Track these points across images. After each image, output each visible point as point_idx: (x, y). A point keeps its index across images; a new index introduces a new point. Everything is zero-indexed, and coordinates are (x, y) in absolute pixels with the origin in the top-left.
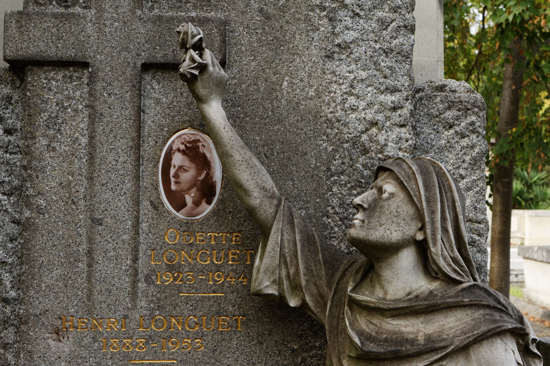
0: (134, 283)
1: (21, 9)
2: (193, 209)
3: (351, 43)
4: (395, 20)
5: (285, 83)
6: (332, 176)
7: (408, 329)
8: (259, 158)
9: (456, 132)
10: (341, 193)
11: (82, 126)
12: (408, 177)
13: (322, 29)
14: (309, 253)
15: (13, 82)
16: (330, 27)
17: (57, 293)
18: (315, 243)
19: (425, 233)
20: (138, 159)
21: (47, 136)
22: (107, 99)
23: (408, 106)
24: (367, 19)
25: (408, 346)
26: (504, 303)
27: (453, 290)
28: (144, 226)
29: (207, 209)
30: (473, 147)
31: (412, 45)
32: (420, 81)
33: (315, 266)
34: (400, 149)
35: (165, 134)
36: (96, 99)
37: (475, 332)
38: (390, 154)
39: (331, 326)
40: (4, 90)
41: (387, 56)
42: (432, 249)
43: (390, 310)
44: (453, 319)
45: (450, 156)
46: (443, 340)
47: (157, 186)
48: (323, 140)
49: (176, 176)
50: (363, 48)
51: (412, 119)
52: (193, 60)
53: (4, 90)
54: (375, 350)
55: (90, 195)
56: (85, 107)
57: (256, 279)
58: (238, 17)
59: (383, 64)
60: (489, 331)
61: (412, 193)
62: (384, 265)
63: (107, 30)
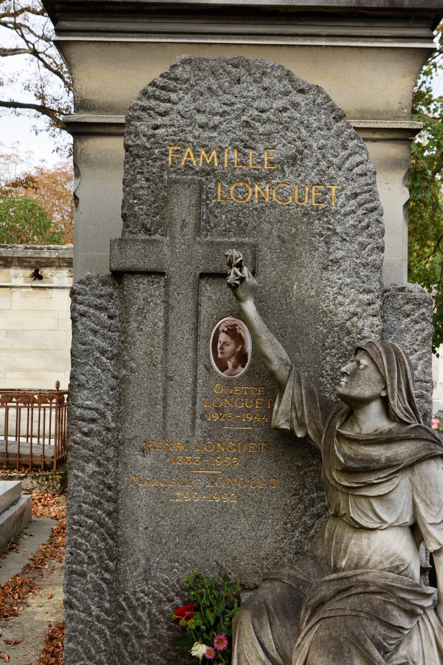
0: (193, 420)
1: (121, 237)
2: (233, 371)
3: (340, 259)
4: (370, 243)
5: (295, 286)
6: (326, 350)
7: (375, 453)
8: (277, 337)
9: (412, 320)
10: (332, 362)
11: (160, 314)
12: (377, 355)
13: (320, 249)
14: (311, 403)
15: (114, 284)
16: (326, 248)
17: (143, 425)
18: (315, 395)
19: (387, 392)
20: (197, 337)
21: (137, 321)
22: (177, 297)
23: (379, 302)
24: (351, 242)
25: (375, 464)
26: (439, 438)
27: (405, 429)
28: (200, 381)
29: (242, 371)
30: (423, 330)
31: (382, 261)
32: (387, 285)
33: (315, 411)
34: (373, 332)
35: (214, 320)
36: (169, 297)
37: (418, 456)
38: (366, 335)
39: (325, 450)
40: (108, 289)
41: (365, 268)
42: (391, 402)
43: (364, 440)
44: (404, 447)
45: (408, 336)
46: (397, 460)
47: (209, 355)
48: (320, 325)
49: (222, 348)
50: (349, 262)
51: (381, 311)
52: (236, 274)
53: (108, 289)
54: (354, 466)
55: (165, 361)
56: (162, 302)
57: (275, 419)
58: (264, 241)
59: (362, 274)
60: (427, 455)
61: (379, 366)
62: (360, 411)
63: (177, 250)
